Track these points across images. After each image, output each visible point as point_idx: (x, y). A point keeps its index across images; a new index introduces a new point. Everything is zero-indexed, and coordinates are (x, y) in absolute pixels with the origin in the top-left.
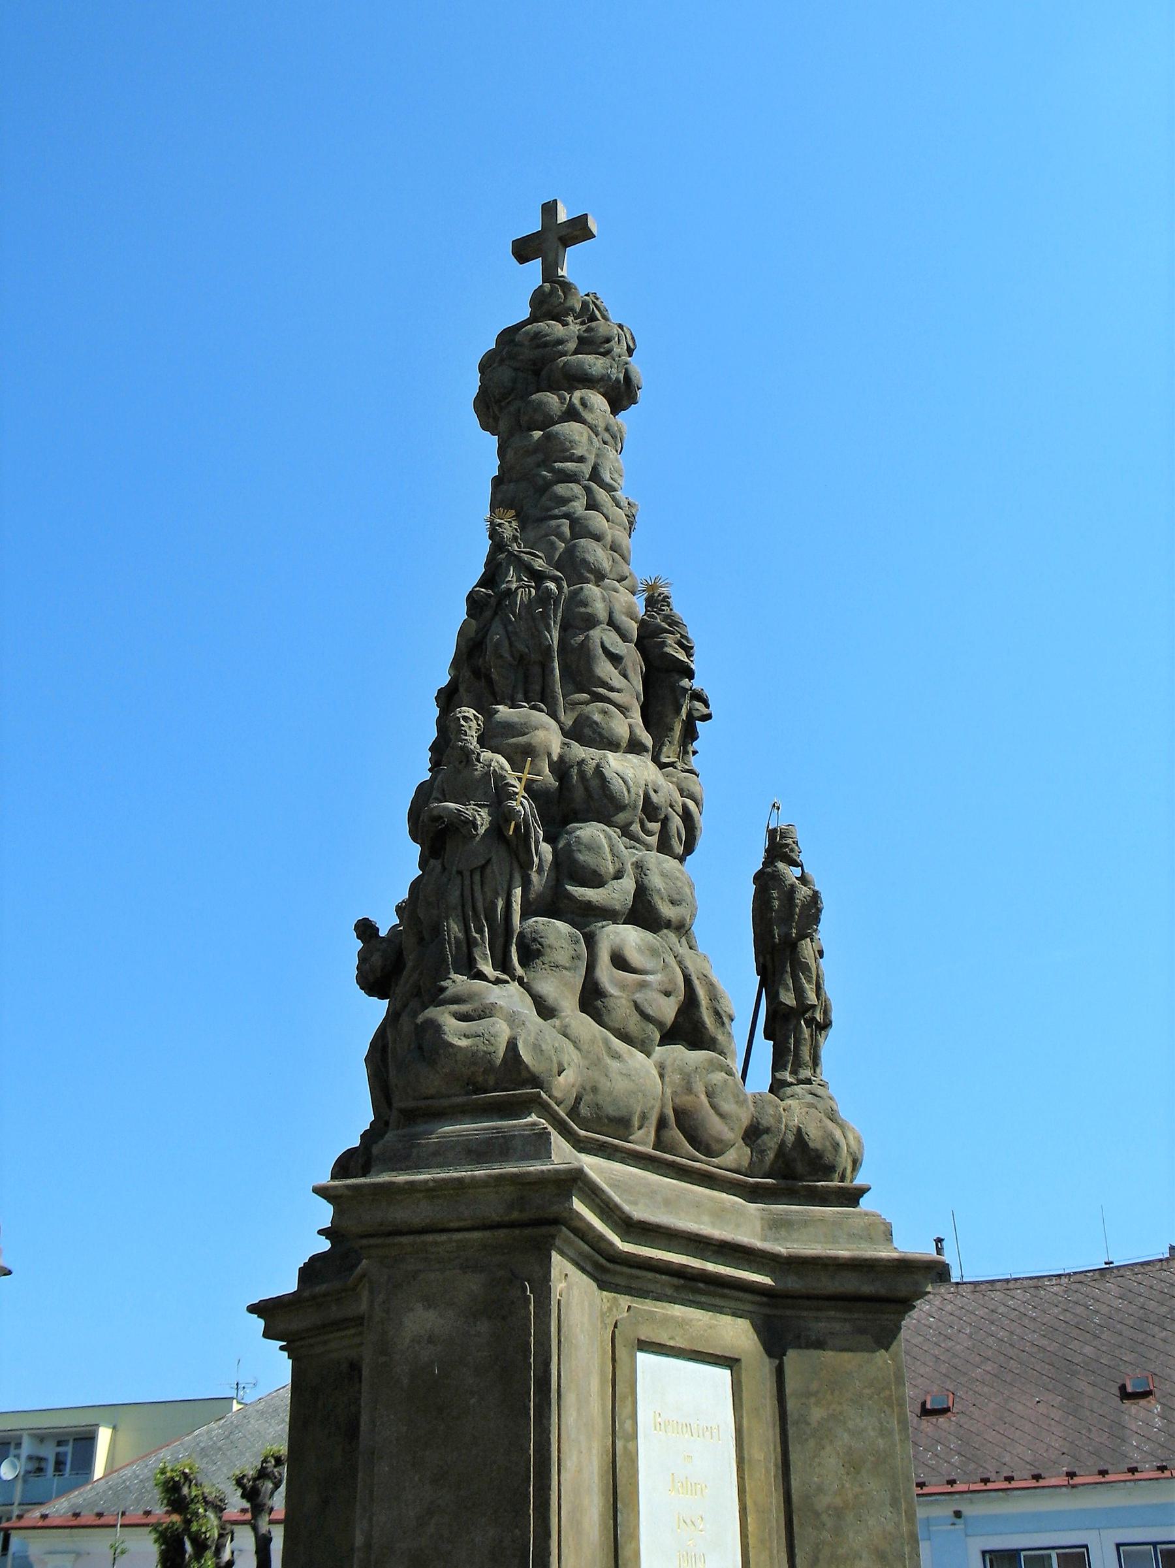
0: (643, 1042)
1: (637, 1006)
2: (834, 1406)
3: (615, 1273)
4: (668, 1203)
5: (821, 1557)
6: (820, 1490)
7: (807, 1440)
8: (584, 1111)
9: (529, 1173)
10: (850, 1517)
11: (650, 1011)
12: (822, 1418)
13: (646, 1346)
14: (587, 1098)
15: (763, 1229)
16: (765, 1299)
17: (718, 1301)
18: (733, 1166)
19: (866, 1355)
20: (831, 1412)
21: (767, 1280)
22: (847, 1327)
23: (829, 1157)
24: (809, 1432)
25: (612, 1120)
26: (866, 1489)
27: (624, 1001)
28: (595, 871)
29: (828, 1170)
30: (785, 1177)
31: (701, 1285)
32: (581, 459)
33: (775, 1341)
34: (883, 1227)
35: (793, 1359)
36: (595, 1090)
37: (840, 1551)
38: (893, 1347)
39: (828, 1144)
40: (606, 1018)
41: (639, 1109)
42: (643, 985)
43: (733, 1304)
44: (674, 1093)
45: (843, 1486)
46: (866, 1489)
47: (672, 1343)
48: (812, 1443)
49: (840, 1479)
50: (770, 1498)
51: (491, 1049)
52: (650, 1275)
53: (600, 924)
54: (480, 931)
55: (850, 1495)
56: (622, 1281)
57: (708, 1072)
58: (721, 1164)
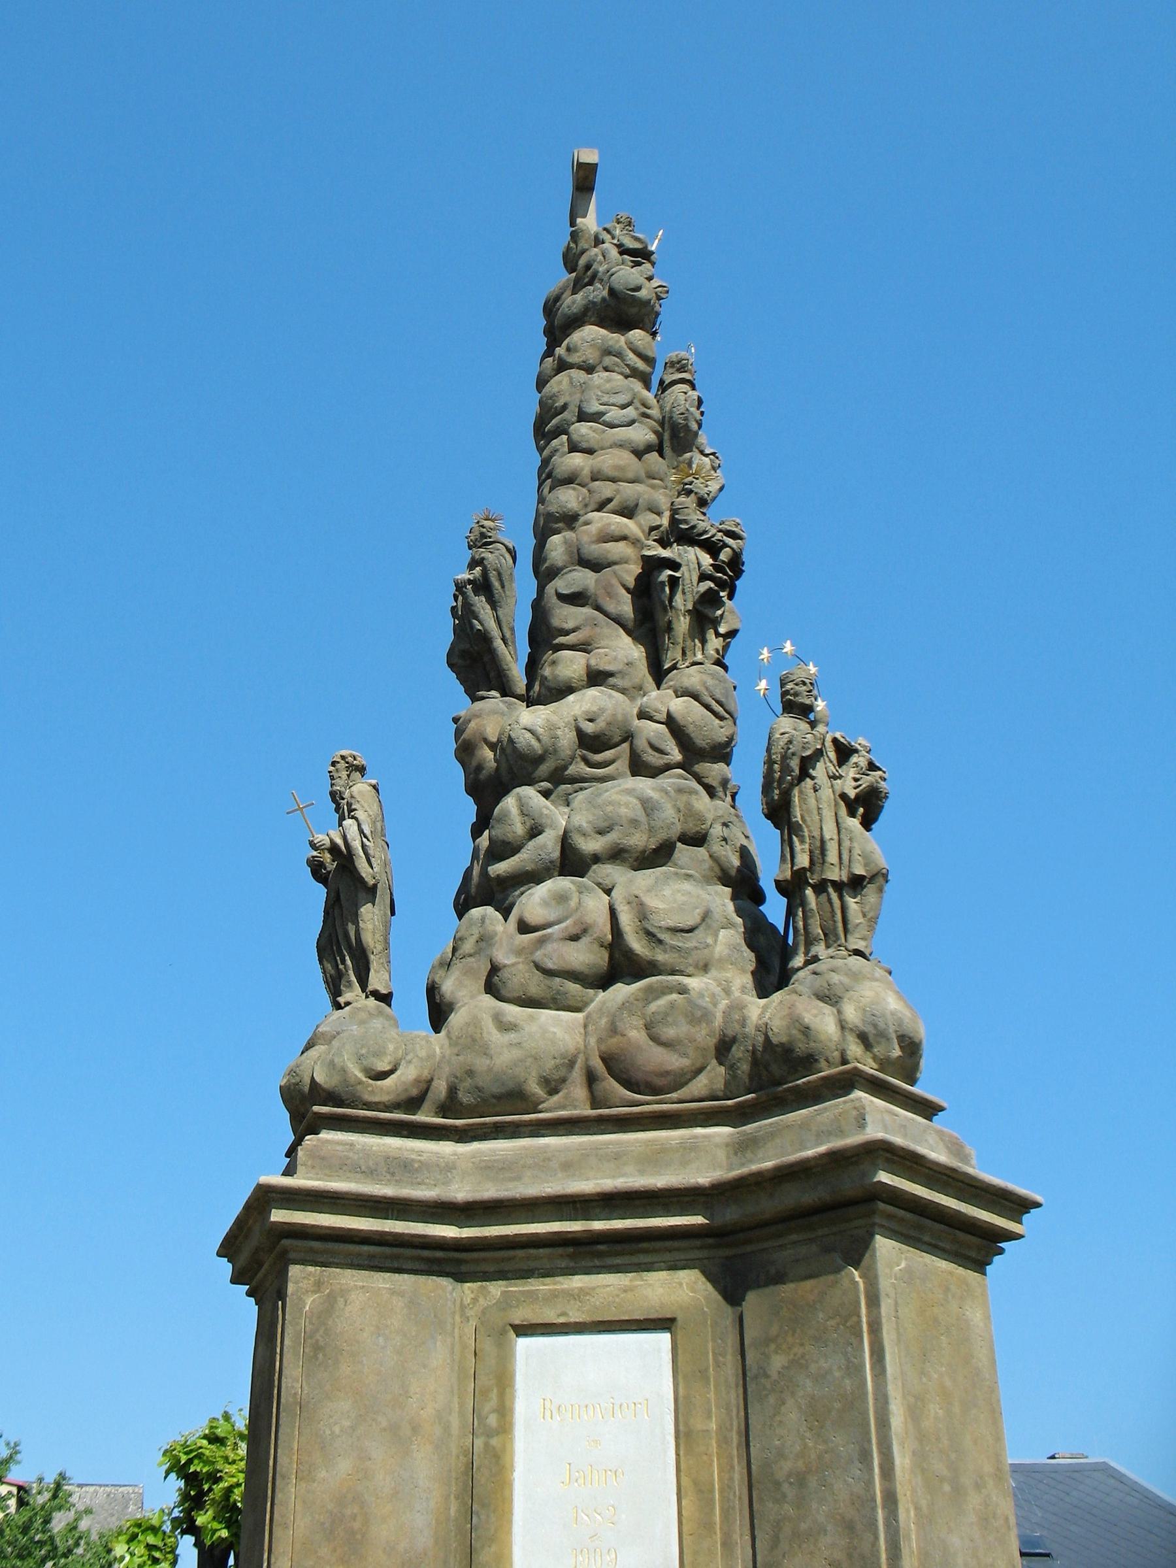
0: (554, 1000)
1: (538, 967)
2: (795, 1350)
3: (466, 1262)
4: (568, 1167)
5: (781, 1536)
6: (781, 1455)
7: (766, 1396)
8: (465, 1098)
10: (813, 1482)
11: (550, 965)
12: (784, 1367)
13: (524, 1330)
15: (728, 1158)
16: (710, 1241)
17: (642, 1258)
18: (704, 1092)
19: (831, 1277)
20: (792, 1357)
21: (699, 1220)
22: (814, 1248)
23: (801, 1047)
24: (768, 1386)
25: (499, 1098)
26: (831, 1445)
28: (503, 842)
29: (808, 1062)
30: (761, 1089)
32: (565, 407)
33: (732, 1286)
34: (854, 1113)
35: (753, 1300)
36: (470, 1073)
37: (803, 1526)
38: (866, 1261)
39: (794, 1032)
40: (504, 992)
42: (542, 942)
43: (667, 1256)
44: (600, 1040)
45: (805, 1446)
46: (831, 1445)
47: (562, 1320)
48: (772, 1400)
49: (803, 1438)
50: (721, 1471)
51: (298, 1079)
52: (520, 1253)
53: (517, 893)
54: (343, 962)
55: (813, 1456)
56: (491, 1268)
57: (647, 1002)
58: (683, 1097)
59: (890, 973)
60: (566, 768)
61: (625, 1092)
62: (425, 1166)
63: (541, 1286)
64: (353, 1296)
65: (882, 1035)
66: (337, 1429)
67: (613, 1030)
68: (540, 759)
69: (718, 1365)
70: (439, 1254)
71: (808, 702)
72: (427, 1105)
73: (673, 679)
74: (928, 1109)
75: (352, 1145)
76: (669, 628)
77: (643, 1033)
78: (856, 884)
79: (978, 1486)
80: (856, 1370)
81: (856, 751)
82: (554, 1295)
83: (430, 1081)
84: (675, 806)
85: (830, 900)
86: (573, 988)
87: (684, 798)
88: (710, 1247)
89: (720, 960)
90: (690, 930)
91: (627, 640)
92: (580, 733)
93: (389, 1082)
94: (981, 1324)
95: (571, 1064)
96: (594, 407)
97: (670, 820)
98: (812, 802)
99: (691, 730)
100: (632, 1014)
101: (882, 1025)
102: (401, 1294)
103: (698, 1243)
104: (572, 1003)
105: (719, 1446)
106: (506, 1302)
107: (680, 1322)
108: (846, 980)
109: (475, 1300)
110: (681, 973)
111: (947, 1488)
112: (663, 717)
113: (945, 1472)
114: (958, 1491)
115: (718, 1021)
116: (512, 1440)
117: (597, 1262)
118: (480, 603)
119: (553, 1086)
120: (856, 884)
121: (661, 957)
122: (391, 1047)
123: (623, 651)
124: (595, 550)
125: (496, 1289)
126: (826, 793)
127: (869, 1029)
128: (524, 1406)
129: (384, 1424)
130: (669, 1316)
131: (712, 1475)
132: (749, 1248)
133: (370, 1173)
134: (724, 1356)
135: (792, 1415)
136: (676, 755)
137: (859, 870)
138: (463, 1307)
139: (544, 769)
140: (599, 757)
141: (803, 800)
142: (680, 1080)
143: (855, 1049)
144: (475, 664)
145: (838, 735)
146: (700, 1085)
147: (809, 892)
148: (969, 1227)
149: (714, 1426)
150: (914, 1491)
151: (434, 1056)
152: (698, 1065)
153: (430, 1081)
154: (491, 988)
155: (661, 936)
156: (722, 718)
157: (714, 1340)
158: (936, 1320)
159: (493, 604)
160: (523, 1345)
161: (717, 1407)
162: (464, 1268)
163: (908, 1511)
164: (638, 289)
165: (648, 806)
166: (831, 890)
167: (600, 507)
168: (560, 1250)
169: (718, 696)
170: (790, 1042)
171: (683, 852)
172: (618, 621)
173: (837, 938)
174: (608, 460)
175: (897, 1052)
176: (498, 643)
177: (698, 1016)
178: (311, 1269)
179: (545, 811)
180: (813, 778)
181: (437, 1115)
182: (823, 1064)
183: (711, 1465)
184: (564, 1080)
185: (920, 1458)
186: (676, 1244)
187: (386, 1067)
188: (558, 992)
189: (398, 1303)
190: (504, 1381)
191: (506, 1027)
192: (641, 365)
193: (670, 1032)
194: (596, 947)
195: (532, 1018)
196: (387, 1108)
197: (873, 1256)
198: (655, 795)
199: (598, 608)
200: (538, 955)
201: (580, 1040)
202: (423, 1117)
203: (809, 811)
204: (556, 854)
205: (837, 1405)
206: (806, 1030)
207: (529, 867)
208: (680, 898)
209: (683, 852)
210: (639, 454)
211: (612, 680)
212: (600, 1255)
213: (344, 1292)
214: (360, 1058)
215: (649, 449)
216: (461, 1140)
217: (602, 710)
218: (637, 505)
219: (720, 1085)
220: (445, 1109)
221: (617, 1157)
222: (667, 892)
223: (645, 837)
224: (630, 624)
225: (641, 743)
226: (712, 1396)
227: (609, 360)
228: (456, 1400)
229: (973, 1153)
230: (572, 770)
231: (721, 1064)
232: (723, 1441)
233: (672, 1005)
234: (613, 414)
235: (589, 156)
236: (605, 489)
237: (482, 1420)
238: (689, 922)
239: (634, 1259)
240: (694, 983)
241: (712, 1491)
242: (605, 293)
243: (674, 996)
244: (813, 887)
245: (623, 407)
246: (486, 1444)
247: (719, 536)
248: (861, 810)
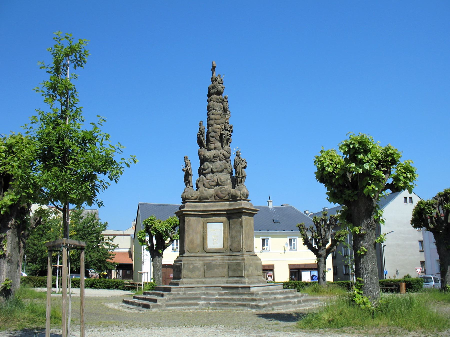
61: (218, 198)
67: (217, 192)
74: (249, 201)
125: (205, 219)
126: (240, 167)
139: (210, 160)
143: (242, 196)
146: (226, 198)
160: (208, 224)
171: (225, 170)
177: (226, 191)
190: (206, 228)
193: (223, 192)
202: (196, 201)
240: (225, 187)
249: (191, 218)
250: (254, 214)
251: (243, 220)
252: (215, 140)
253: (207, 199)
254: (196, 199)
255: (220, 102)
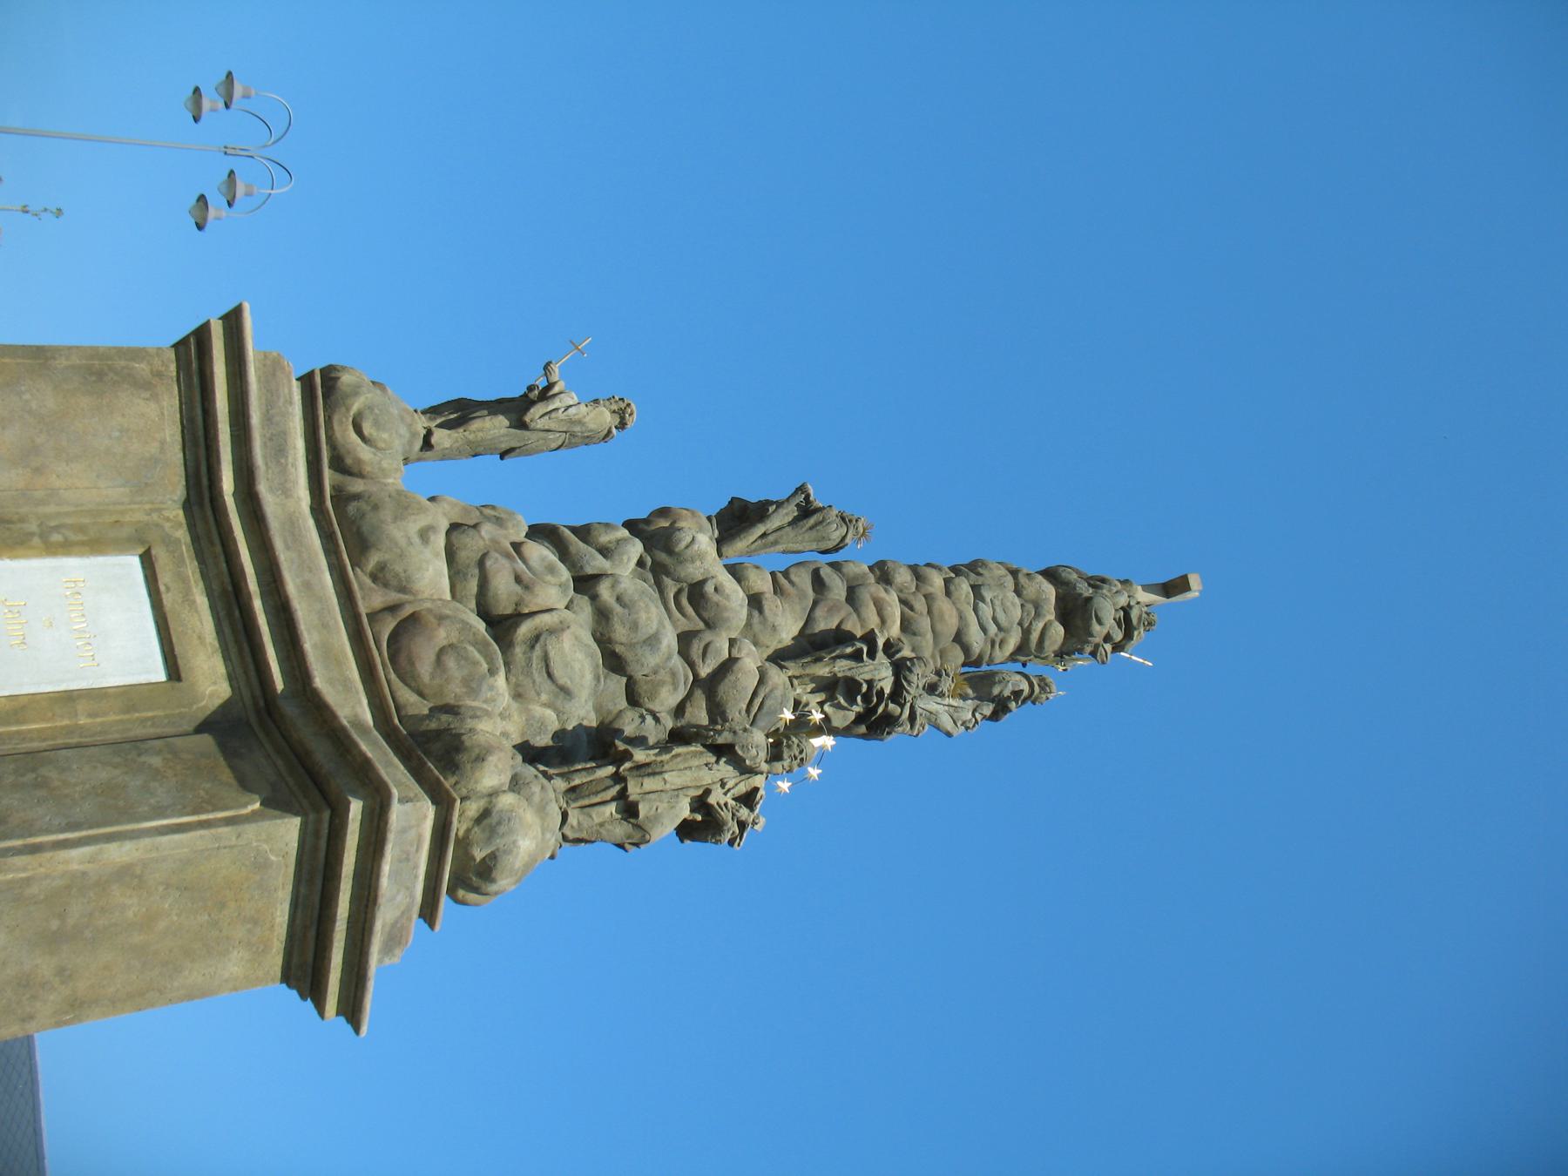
0: (458, 572)
8: (352, 508)
9: (356, 745)
11: (488, 563)
13: (147, 561)
14: (363, 505)
16: (262, 703)
17: (233, 650)
18: (401, 700)
21: (279, 685)
23: (463, 758)
27: (481, 543)
31: (237, 613)
36: (376, 507)
41: (387, 556)
42: (508, 556)
43: (239, 671)
44: (429, 610)
45: (76, 785)
47: (162, 588)
48: (117, 760)
52: (219, 549)
57: (475, 644)
59: (552, 857)
60: (668, 574)
61: (388, 638)
62: (284, 470)
63: (191, 569)
64: (153, 405)
65: (492, 832)
66: (27, 396)
67: (441, 618)
68: (670, 551)
69: (143, 721)
70: (205, 482)
71: (785, 755)
72: (339, 477)
73: (773, 671)
74: (428, 912)
75: (291, 403)
76: (819, 660)
77: (445, 643)
78: (630, 811)
79: (60, 971)
80: (159, 812)
81: (752, 810)
82: (184, 580)
83: (361, 475)
84: (658, 666)
85: (607, 788)
86: (473, 586)
87: (668, 678)
88: (256, 704)
89: (527, 710)
90: (550, 675)
91: (795, 631)
92: (703, 582)
93: (354, 436)
94: (227, 975)
95: (403, 589)
96: (988, 595)
97: (646, 663)
98: (695, 762)
99: (731, 677)
100: (461, 631)
101: (502, 829)
102: (162, 450)
103: (258, 693)
104: (459, 587)
105: (63, 728)
106: (169, 542)
107: (177, 685)
108: (537, 798)
109: (168, 519)
110: (508, 671)
111: (55, 924)
112: (735, 654)
113: (71, 922)
114: (52, 941)
115: (469, 703)
116: (39, 555)
117: (222, 614)
118: (791, 511)
119: (379, 576)
120: (630, 811)
121: (519, 650)
122: (385, 436)
123: (788, 628)
124: (865, 595)
125: (182, 534)
126: (707, 778)
127: (494, 819)
128: (75, 566)
129: (38, 441)
130: (183, 675)
131: (34, 722)
132: (261, 735)
133: (268, 419)
134: (153, 725)
135: (104, 774)
136: (705, 671)
137: (643, 810)
138: (159, 510)
139: (663, 557)
140: (685, 601)
141: (695, 755)
142: (408, 677)
143: (473, 808)
144: (737, 519)
145: (762, 792)
146: (407, 696)
147: (611, 769)
148: (320, 955)
149: (83, 721)
150: (47, 876)
151: (386, 476)
152: (426, 691)
153: (361, 475)
154: (454, 527)
155: (538, 647)
156: (748, 711)
157: (166, 716)
158: (223, 905)
159: (794, 522)
160: (134, 562)
161: (102, 724)
162: (195, 508)
163: (24, 869)
164: (1100, 622)
165: (653, 641)
166: (618, 787)
167: (903, 602)
168: (227, 580)
169: (768, 703)
170: (466, 749)
171: (617, 684)
172: (809, 620)
173: (575, 800)
174: (943, 604)
175: (479, 854)
176: (760, 529)
177: (472, 685)
178: (173, 367)
179: (625, 558)
180: (717, 762)
181: (333, 487)
182: (452, 780)
183: (43, 720)
184: (386, 585)
185: (77, 884)
186: (253, 673)
187: (367, 428)
188: (465, 575)
189: (153, 448)
190: (95, 543)
191: (425, 534)
192: (1035, 636)
193: (450, 662)
194: (515, 599)
195: (437, 555)
196: (330, 438)
197: (276, 817)
198: (665, 643)
199: (815, 603)
200: (494, 555)
201: (426, 595)
202: (328, 475)
203: (685, 760)
204: (589, 571)
205: (121, 803)
206: (481, 759)
207: (572, 549)
208: (577, 666)
209: (617, 684)
210: (959, 638)
211: (756, 613)
212: (230, 615)
213: (155, 397)
214: (371, 408)
215: (966, 649)
216: (312, 509)
217: (728, 598)
218: (914, 634)
219: (411, 711)
220: (341, 498)
221: (325, 626)
222: (580, 656)
223: (624, 640)
224: (808, 632)
225: (708, 636)
226: (112, 718)
227: (1030, 607)
228: (72, 509)
229: (396, 960)
230: (667, 581)
231: (431, 710)
232: (69, 731)
233: (476, 663)
234: (986, 610)
235: (1194, 581)
236: (920, 604)
237: (57, 528)
238: (558, 672)
239: (231, 645)
240: (500, 680)
241: (18, 722)
242: (1086, 594)
243: (485, 666)
244: (617, 773)
245: (994, 619)
246: (32, 534)
247: (909, 698)
248: (699, 818)
249: (170, 402)
250: (313, 989)
251: (250, 830)
252: (802, 596)
253: (361, 544)
254: (339, 464)
255: (1026, 633)
